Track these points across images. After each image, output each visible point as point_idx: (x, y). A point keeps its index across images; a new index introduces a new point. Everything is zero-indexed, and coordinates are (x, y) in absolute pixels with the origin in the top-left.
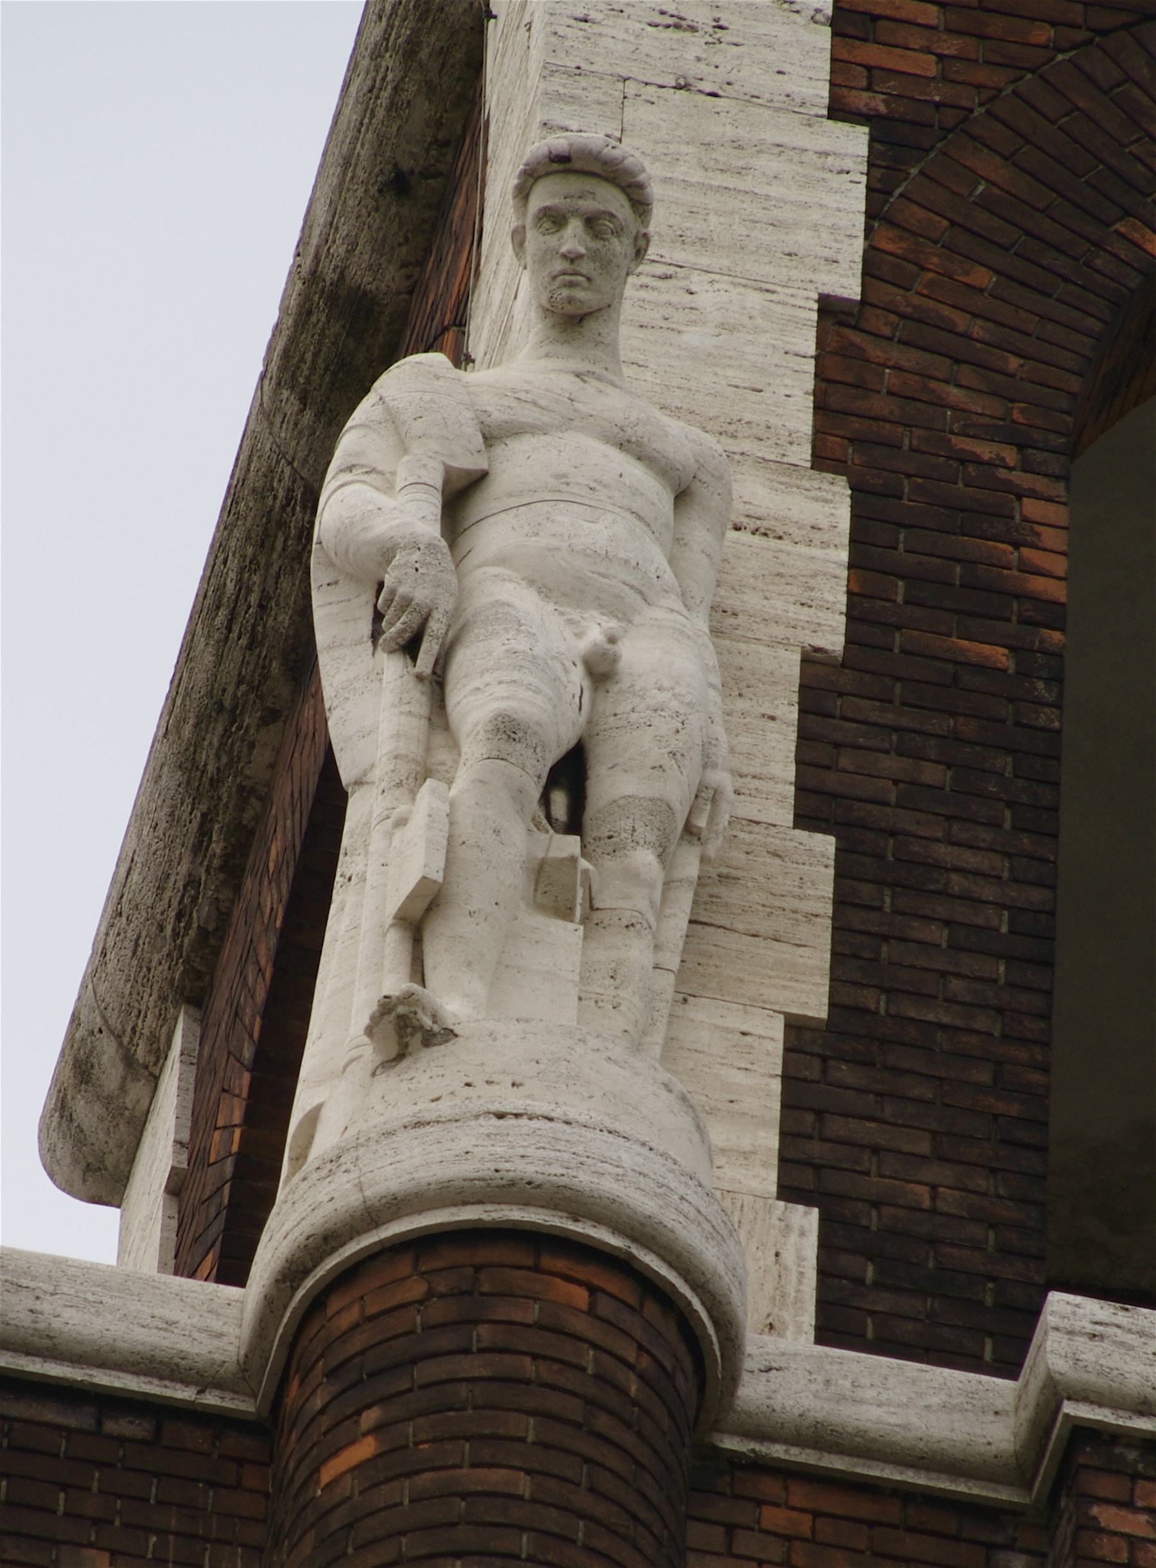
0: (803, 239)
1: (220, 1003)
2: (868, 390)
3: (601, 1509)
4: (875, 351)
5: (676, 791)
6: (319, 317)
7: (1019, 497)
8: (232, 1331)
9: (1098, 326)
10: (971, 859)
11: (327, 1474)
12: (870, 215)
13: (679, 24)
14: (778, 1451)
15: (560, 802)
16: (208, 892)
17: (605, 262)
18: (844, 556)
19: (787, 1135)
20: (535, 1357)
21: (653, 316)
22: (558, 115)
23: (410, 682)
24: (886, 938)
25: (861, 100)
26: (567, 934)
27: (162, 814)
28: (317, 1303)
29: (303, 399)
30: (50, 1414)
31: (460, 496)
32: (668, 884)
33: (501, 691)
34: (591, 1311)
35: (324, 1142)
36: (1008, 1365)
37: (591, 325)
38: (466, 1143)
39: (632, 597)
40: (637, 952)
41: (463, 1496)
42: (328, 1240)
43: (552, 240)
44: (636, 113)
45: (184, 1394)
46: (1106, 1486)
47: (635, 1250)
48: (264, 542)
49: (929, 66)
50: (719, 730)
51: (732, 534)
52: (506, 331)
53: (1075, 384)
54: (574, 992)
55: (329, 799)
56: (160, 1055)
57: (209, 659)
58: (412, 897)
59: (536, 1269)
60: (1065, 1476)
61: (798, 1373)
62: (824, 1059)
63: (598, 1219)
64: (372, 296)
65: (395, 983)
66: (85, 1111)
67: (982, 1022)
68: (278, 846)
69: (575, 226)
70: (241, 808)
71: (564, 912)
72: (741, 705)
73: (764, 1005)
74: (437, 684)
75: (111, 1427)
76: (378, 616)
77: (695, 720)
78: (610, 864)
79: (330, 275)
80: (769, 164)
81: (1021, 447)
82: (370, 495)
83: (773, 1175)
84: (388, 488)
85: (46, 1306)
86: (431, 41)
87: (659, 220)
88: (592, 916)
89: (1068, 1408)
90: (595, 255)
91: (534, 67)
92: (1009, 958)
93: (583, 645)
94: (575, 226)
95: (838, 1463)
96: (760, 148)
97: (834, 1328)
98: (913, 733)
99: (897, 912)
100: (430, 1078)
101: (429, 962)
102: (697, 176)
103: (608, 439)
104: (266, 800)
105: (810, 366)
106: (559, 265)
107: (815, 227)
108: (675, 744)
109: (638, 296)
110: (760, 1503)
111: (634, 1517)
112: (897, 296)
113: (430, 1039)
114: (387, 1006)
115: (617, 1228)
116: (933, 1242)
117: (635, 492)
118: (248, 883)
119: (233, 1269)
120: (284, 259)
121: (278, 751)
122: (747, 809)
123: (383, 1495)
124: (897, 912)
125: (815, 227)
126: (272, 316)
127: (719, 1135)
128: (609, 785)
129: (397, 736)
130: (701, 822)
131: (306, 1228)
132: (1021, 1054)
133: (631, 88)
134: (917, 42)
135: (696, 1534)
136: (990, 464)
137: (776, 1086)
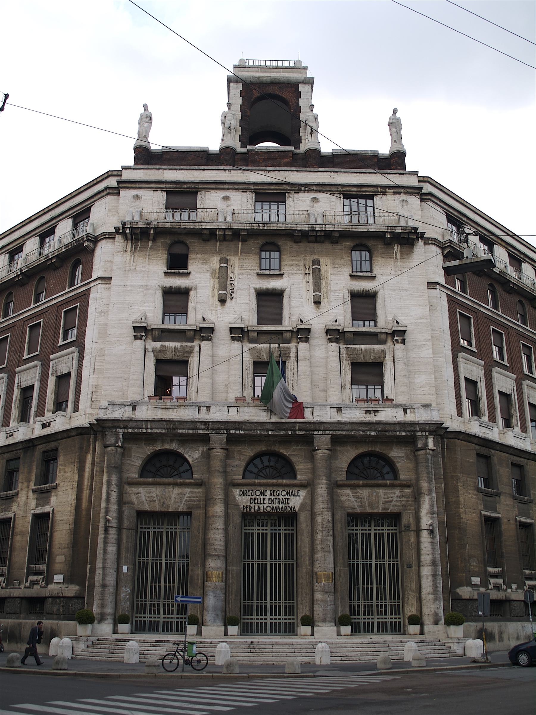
61: (239, 149)
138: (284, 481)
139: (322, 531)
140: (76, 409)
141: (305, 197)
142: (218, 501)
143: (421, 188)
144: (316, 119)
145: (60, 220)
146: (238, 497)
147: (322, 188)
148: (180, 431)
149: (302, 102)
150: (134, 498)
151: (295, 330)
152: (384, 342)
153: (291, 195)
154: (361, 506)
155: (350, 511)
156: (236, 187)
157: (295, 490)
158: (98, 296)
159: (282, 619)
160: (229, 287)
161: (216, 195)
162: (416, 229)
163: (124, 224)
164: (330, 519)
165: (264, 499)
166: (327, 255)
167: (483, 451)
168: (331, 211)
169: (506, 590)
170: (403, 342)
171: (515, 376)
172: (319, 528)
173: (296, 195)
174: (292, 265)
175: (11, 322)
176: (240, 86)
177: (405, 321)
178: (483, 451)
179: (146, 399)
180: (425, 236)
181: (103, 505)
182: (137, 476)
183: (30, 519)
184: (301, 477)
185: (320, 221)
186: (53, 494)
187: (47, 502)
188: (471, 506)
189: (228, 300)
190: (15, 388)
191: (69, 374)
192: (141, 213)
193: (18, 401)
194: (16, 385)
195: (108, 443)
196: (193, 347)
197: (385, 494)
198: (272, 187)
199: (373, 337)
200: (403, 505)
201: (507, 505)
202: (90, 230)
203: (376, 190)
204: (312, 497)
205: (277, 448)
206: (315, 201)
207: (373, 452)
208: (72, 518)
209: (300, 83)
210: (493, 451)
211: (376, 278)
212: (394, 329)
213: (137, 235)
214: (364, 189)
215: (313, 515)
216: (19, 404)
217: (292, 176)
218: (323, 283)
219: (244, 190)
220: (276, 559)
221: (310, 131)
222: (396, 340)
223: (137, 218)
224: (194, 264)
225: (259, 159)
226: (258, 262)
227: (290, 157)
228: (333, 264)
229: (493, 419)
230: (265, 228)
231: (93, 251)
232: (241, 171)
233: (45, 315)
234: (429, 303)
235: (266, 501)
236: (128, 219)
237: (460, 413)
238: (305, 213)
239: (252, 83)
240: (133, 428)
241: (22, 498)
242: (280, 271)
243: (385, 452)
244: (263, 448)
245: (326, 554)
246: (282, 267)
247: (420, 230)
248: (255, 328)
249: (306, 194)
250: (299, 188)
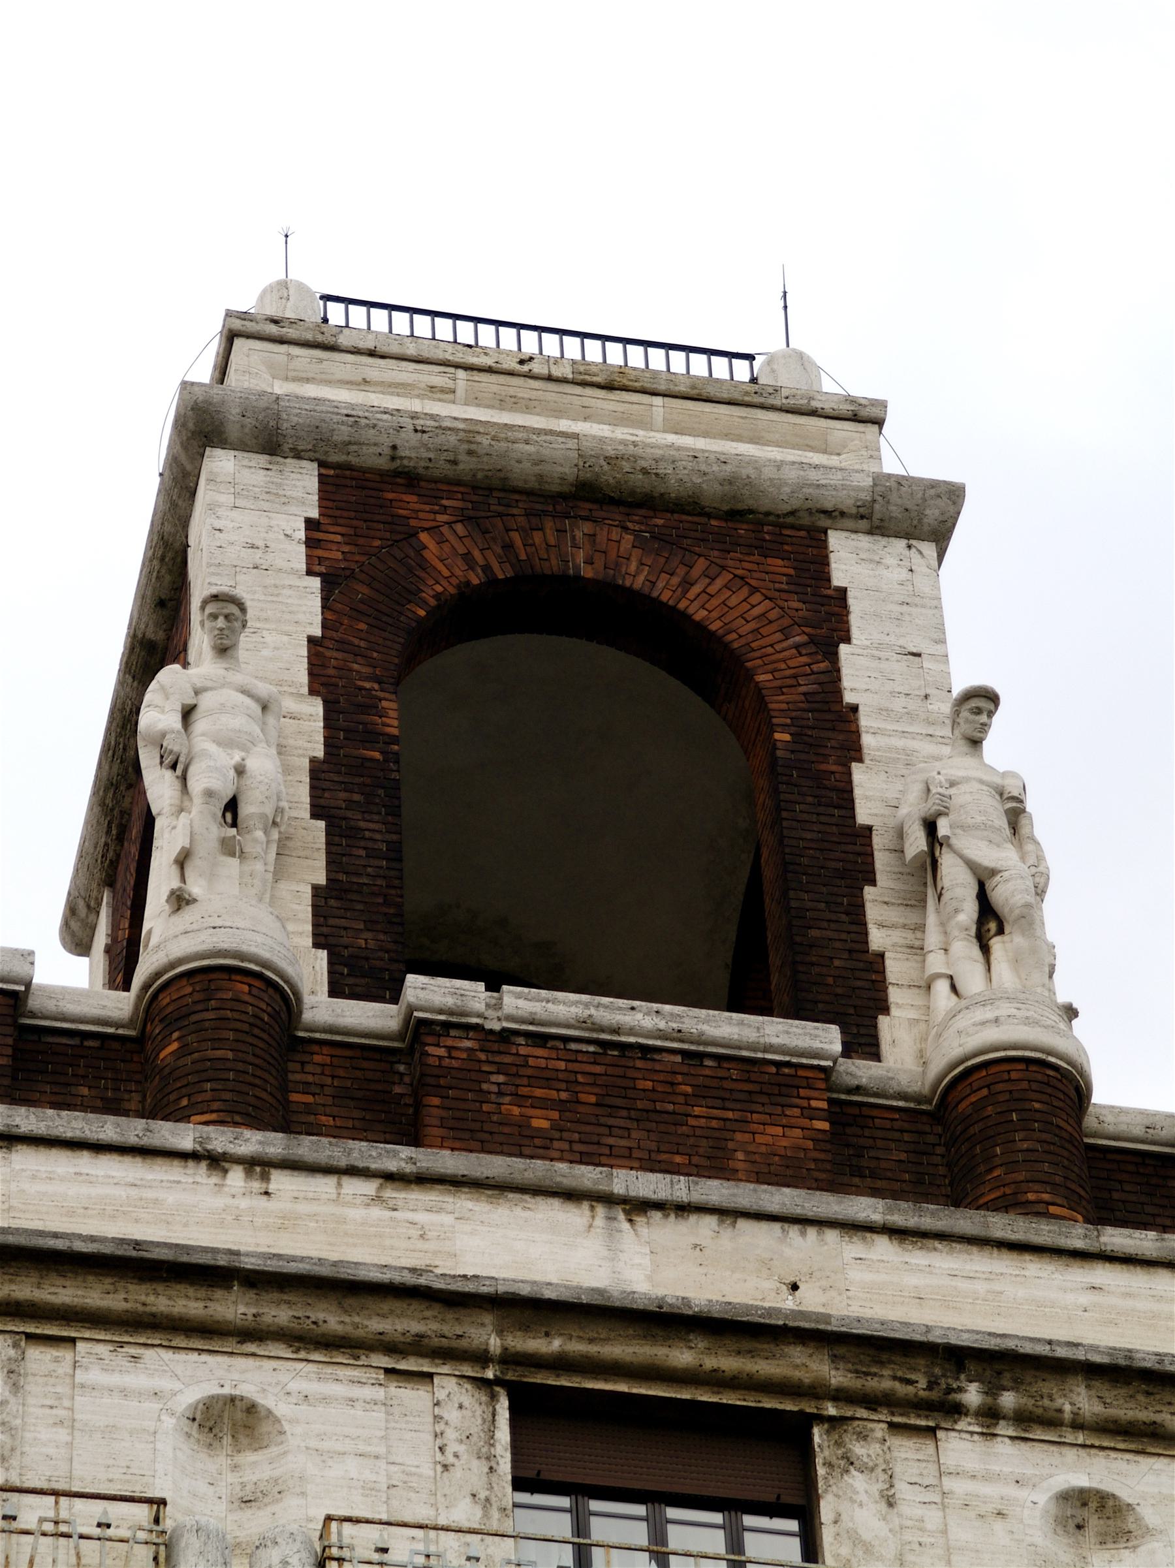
0: (301, 617)
1: (118, 885)
2: (326, 668)
3: (257, 1061)
4: (328, 653)
5: (269, 810)
6: (137, 650)
7: (380, 700)
8: (126, 1007)
9: (402, 641)
10: (372, 826)
11: (162, 1056)
12: (323, 607)
13: (253, 547)
14: (317, 1035)
15: (229, 816)
16: (112, 848)
17: (233, 630)
18: (322, 724)
19: (315, 925)
20: (231, 1010)
21: (251, 646)
22: (213, 580)
23: (174, 779)
24: (344, 855)
25: (317, 568)
26: (234, 862)
27: (95, 822)
28: (155, 996)
29: (134, 677)
30: (64, 1041)
31: (188, 714)
32: (268, 842)
33: (206, 780)
34: (250, 993)
35: (154, 941)
36: (395, 1000)
37: (229, 652)
38: (203, 938)
39: (249, 744)
40: (259, 867)
41: (209, 1060)
42: (158, 975)
43: (214, 624)
44: (240, 578)
45: (111, 1030)
46: (429, 1039)
47: (264, 971)
48: (124, 727)
49: (339, 556)
50: (282, 787)
51: (283, 719)
52: (201, 653)
53: (396, 661)
54: (237, 882)
55: (149, 821)
56: (99, 904)
57: (107, 767)
58: (179, 854)
59: (230, 980)
60: (416, 1037)
61: (323, 1009)
62: (326, 898)
63: (250, 961)
64: (155, 645)
65: (176, 884)
66: (75, 925)
67: (379, 882)
68: (135, 831)
69: (221, 619)
70: (122, 818)
71: (233, 855)
72: (289, 778)
73: (303, 881)
74: (184, 779)
75: (86, 1043)
76: (162, 757)
77: (274, 785)
78: (247, 836)
79: (140, 636)
80: (286, 592)
81: (379, 683)
82: (157, 714)
83: (310, 940)
84: (163, 712)
85: (60, 1004)
86: (170, 555)
87: (250, 614)
88: (242, 855)
89: (416, 1014)
90: (229, 628)
91: (204, 564)
92: (387, 859)
93: (233, 762)
94: (221, 619)
95: (338, 1038)
96: (284, 587)
97: (335, 991)
98: (349, 784)
99: (348, 846)
100: (189, 915)
101: (186, 875)
102: (263, 598)
103: (237, 690)
104: (130, 815)
105: (306, 660)
106: (217, 632)
107: (304, 613)
108: (267, 794)
109: (245, 640)
110: (312, 1054)
111: (269, 1063)
112: (334, 634)
113: (188, 903)
114: (173, 892)
115: (257, 964)
116: (367, 959)
117: (248, 708)
118: (126, 844)
119: (127, 988)
120: (125, 631)
121: (133, 798)
122: (294, 814)
123: (181, 1062)
124: (348, 846)
125: (304, 613)
126: (122, 650)
127: (290, 927)
128: (245, 810)
129: (171, 798)
130: (278, 820)
131: (150, 971)
132: (393, 892)
133: (238, 569)
134: (334, 548)
135: (291, 1066)
136: (369, 690)
137: (310, 909)
144: (1016, 816)
149: (861, 673)
153: (859, 1449)
161: (136, 1379)
173: (907, 1454)
176: (302, 487)
198: (682, 1356)
206: (1094, 1523)
209: (836, 515)
216: (312, 1273)
217: (857, 1275)
219: (409, 1360)
221: (969, 912)
225: (520, 1099)
227: (810, 1113)
232: (369, 1187)
239: (404, 477)
249: (1007, 1456)
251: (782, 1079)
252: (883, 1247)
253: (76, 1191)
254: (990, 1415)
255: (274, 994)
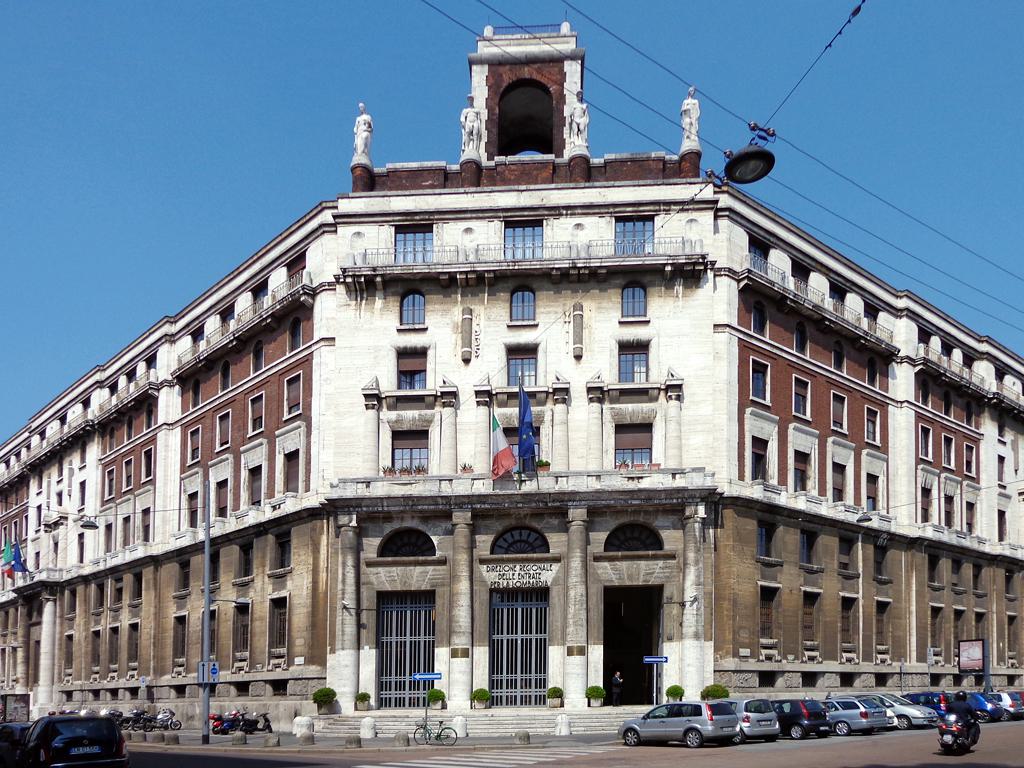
61: (485, 162)
138: (535, 555)
139: (575, 605)
140: (307, 489)
141: (567, 223)
142: (462, 578)
143: (716, 202)
145: (273, 270)
146: (485, 573)
147: (589, 209)
148: (420, 507)
150: (373, 579)
151: (551, 390)
152: (431, 406)
154: (620, 579)
155: (607, 584)
156: (481, 215)
157: (547, 565)
158: (325, 363)
159: (533, 692)
160: (474, 343)
162: (703, 257)
163: (344, 270)
164: (584, 593)
165: (513, 575)
166: (593, 298)
167: (767, 517)
168: (587, 238)
169: (780, 661)
170: (679, 398)
171: (818, 432)
172: (572, 601)
174: (549, 312)
175: (230, 395)
177: (684, 373)
178: (767, 517)
179: (381, 474)
180: (716, 266)
181: (340, 586)
182: (376, 555)
183: (268, 604)
184: (553, 551)
185: (583, 254)
186: (289, 578)
187: (283, 586)
188: (745, 577)
189: (473, 359)
190: (242, 469)
191: (297, 451)
192: (365, 255)
193: (247, 483)
194: (242, 466)
195: (340, 523)
196: (433, 416)
197: (646, 566)
198: (526, 213)
199: (642, 394)
200: (666, 577)
201: (791, 575)
202: (306, 281)
203: (657, 208)
204: (566, 572)
205: (528, 522)
207: (633, 523)
208: (309, 601)
210: (779, 517)
211: (651, 324)
212: (668, 383)
213: (363, 285)
214: (641, 208)
215: (567, 589)
218: (586, 333)
219: (601, 215)
220: (527, 633)
221: (576, 130)
222: (670, 396)
223: (359, 263)
224: (432, 317)
226: (508, 310)
228: (599, 308)
229: (783, 480)
230: (516, 267)
231: (311, 308)
233: (266, 386)
234: (715, 349)
235: (516, 576)
236: (348, 264)
237: (741, 477)
238: (566, 244)
240: (367, 506)
241: (258, 583)
242: (534, 320)
243: (650, 521)
244: (513, 522)
245: (579, 627)
246: (537, 316)
247: (710, 258)
248: (505, 390)
250: (557, 211)
251: (544, 164)
252: (556, 192)
253: (449, 201)
254: (567, 215)
255: (477, 164)
